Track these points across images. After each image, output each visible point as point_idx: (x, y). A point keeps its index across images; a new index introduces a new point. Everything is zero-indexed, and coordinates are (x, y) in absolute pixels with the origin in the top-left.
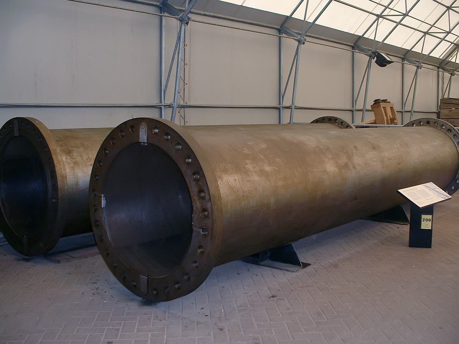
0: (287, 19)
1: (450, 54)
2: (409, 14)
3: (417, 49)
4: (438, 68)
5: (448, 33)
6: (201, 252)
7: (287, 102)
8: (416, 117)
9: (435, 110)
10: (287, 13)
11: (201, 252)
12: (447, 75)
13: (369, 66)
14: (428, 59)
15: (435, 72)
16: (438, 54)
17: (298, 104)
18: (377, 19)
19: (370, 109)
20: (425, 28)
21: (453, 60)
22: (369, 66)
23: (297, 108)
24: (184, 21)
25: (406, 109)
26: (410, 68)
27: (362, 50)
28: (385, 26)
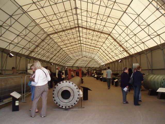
0: (5, 49)
1: (30, 54)
2: (2, 36)
3: (20, 52)
4: (34, 59)
5: (29, 48)
6: (139, 69)
7: (4, 68)
8: (21, 72)
9: (25, 70)
10: (4, 48)
11: (139, 69)
12: (29, 60)
13: (7, 57)
14: (24, 55)
15: (25, 59)
16: (26, 54)
17: (6, 69)
18: (10, 44)
19: (11, 69)
20: (23, 47)
21: (30, 55)
22: (7, 57)
23: (6, 70)
24: (21, 58)
25: (3, 69)
26: (19, 58)
27: (5, 53)
28: (12, 46)
